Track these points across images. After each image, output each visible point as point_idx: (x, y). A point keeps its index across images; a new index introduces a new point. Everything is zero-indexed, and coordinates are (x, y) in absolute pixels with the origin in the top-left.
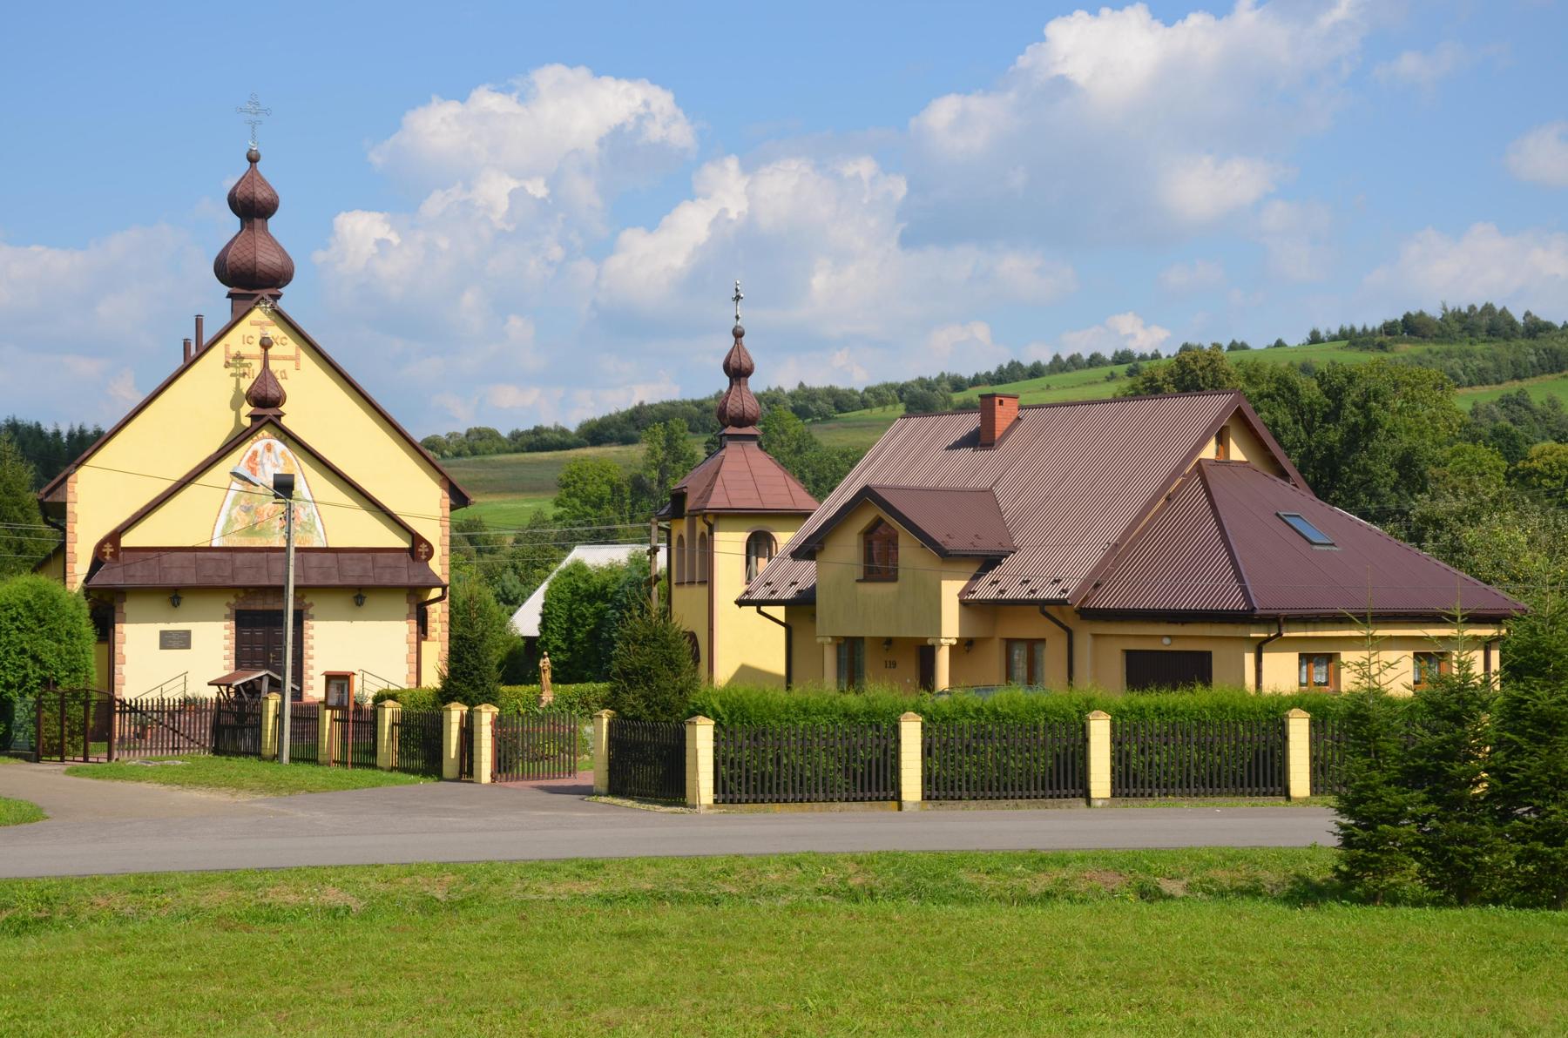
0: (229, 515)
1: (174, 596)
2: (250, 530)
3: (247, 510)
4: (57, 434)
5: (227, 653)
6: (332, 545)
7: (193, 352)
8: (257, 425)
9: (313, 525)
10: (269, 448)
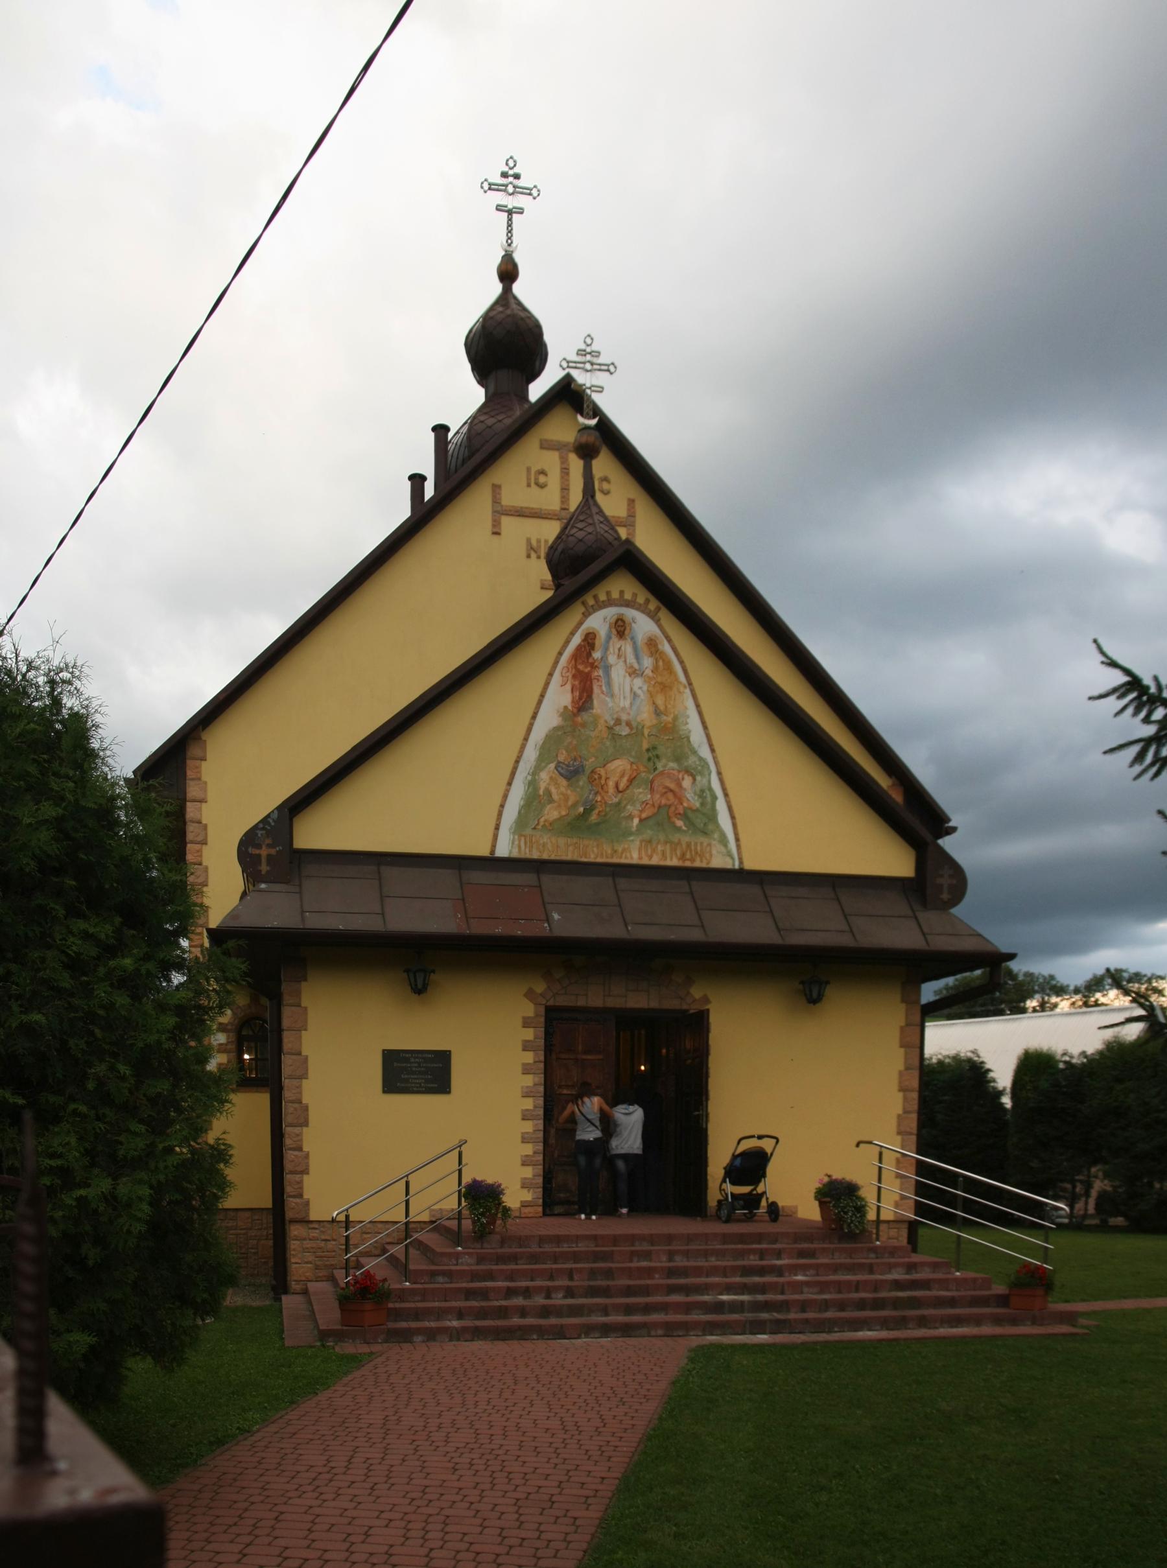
0: (532, 784)
1: (416, 961)
2: (579, 823)
3: (571, 773)
4: (994, 1081)
5: (529, 1104)
6: (749, 865)
7: (429, 491)
8: (570, 584)
9: (712, 817)
10: (620, 628)
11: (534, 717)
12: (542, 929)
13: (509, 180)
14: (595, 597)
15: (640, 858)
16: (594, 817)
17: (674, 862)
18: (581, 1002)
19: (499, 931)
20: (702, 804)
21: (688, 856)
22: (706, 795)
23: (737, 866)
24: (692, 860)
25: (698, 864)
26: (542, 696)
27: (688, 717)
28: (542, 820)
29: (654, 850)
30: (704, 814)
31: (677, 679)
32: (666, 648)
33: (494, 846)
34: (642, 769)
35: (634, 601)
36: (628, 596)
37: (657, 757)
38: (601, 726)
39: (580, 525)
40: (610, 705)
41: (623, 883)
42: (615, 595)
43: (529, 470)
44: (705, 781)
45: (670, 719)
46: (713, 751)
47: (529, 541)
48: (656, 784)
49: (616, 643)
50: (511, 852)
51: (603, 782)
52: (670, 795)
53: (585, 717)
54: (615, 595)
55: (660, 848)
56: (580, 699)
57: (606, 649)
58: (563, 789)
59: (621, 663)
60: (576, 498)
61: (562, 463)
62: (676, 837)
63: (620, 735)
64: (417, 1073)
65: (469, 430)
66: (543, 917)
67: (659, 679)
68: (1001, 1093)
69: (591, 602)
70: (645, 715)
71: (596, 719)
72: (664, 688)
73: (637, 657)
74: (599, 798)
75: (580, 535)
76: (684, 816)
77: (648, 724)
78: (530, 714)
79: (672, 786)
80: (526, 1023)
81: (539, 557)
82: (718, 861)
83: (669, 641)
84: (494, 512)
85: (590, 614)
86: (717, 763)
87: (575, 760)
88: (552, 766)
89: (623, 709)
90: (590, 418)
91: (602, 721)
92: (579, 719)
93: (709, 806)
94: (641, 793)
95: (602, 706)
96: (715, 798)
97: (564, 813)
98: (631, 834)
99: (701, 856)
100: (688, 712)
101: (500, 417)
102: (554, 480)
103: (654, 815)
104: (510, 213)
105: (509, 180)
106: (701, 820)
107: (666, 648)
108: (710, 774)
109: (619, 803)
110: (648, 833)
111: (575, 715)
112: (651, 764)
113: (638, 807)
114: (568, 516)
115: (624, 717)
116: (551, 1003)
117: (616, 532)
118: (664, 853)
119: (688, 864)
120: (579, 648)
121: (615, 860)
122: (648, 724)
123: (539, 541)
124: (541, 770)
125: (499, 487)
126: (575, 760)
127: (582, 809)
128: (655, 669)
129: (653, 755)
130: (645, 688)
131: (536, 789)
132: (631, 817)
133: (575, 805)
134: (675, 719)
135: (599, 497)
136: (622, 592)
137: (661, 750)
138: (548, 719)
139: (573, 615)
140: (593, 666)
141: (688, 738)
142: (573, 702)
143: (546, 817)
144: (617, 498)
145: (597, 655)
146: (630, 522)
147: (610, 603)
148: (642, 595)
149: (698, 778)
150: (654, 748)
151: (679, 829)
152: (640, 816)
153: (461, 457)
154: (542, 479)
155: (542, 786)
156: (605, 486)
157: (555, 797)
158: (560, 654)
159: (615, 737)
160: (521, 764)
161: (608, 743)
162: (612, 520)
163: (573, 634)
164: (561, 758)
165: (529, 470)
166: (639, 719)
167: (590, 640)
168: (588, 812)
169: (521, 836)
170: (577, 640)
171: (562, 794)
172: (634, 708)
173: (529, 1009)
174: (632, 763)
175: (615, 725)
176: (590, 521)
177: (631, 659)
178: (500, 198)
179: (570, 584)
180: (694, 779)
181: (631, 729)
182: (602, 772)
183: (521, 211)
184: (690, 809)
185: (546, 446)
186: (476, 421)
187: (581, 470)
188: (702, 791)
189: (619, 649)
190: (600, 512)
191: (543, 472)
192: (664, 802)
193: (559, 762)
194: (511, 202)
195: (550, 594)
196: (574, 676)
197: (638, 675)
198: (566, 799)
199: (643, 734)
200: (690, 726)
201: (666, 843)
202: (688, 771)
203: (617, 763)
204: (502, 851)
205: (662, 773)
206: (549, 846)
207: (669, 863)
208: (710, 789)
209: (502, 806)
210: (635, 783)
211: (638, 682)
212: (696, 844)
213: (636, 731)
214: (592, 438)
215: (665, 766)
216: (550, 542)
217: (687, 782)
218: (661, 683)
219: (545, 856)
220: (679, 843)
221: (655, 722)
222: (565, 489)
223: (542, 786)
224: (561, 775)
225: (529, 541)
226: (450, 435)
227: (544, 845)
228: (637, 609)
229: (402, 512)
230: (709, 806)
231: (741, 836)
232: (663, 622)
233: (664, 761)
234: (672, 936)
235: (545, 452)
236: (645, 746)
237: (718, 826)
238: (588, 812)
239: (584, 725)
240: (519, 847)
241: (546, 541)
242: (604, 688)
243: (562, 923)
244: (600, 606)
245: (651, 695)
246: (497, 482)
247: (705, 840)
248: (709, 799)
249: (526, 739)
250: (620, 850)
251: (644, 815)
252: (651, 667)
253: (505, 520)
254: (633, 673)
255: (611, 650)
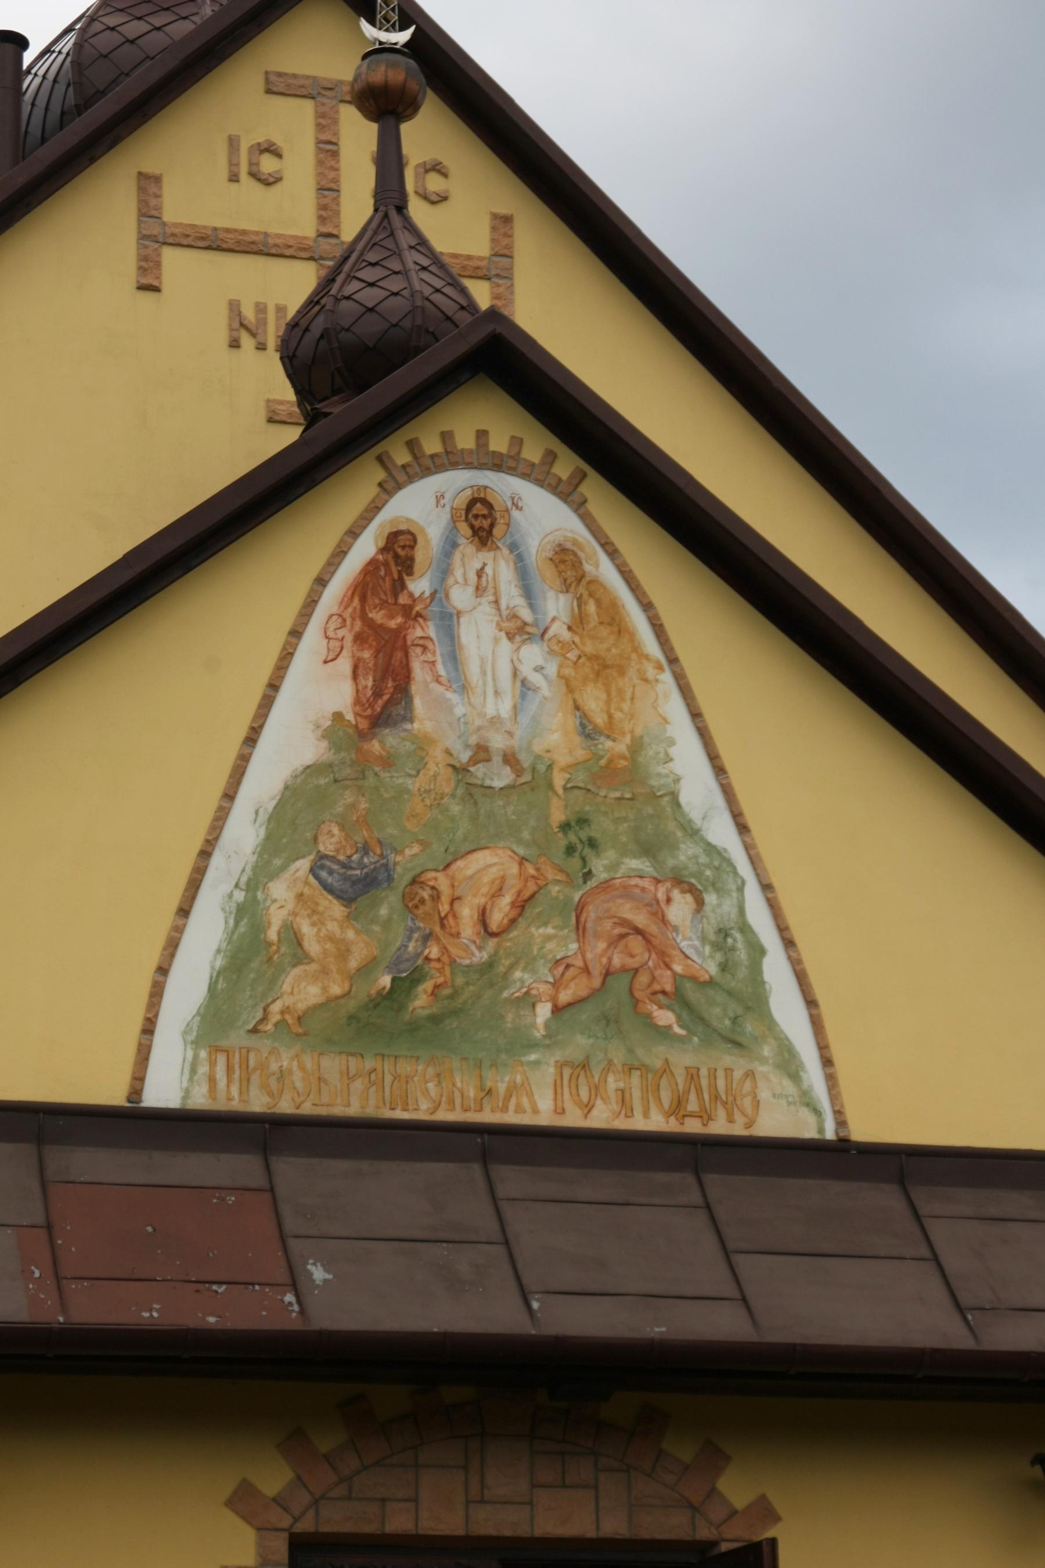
0: (248, 912)
2: (380, 1018)
3: (356, 884)
6: (865, 1130)
8: (345, 412)
9: (754, 1000)
10: (481, 521)
11: (252, 739)
12: (276, 1311)
14: (412, 445)
15: (560, 1111)
16: (421, 1001)
17: (656, 1122)
18: (399, 1522)
19: (151, 1314)
20: (724, 967)
21: (693, 1106)
22: (730, 938)
23: (830, 1134)
24: (705, 1116)
25: (719, 1127)
26: (274, 687)
27: (672, 742)
28: (276, 1007)
29: (596, 1090)
30: (730, 993)
31: (637, 649)
32: (607, 571)
33: (139, 1079)
34: (550, 874)
35: (516, 457)
36: (498, 444)
37: (592, 843)
38: (436, 763)
39: (369, 274)
40: (459, 710)
41: (513, 1179)
42: (465, 441)
43: (233, 143)
44: (728, 907)
45: (621, 747)
46: (743, 829)
47: (234, 307)
48: (591, 913)
49: (470, 559)
50: (185, 1098)
51: (444, 908)
52: (636, 944)
53: (390, 739)
54: (465, 441)
55: (613, 1083)
56: (377, 694)
57: (445, 572)
58: (332, 927)
59: (485, 606)
60: (356, 210)
61: (320, 127)
62: (655, 1055)
63: (485, 789)
65: (78, 46)
66: (281, 1275)
67: (589, 648)
68: (670, 1027)
69: (401, 457)
70: (554, 738)
71: (422, 744)
72: (604, 669)
73: (528, 593)
74: (434, 951)
75: (370, 296)
76: (676, 998)
77: (563, 759)
78: (242, 732)
79: (640, 919)
81: (261, 347)
82: (778, 1120)
83: (613, 553)
84: (142, 237)
85: (399, 487)
86: (755, 861)
87: (366, 849)
88: (303, 865)
89: (495, 721)
90: (392, 28)
91: (438, 753)
92: (375, 746)
93: (742, 973)
94: (550, 938)
95: (438, 713)
96: (758, 951)
97: (336, 990)
98: (532, 1045)
99: (731, 1109)
100: (671, 731)
101: (157, 21)
102: (299, 167)
103: (594, 993)
106: (725, 1009)
107: (607, 571)
108: (741, 889)
109: (490, 965)
110: (580, 1044)
111: (363, 736)
112: (575, 862)
113: (544, 972)
114: (338, 253)
115: (498, 742)
116: (306, 1525)
117: (463, 291)
118: (623, 1096)
119: (693, 1127)
120: (371, 568)
121: (488, 1116)
122: (563, 759)
123: (261, 309)
124: (273, 876)
125: (157, 180)
126: (366, 849)
127: (386, 981)
128: (578, 623)
129: (579, 839)
130: (552, 669)
131: (258, 927)
132: (528, 1000)
133: (367, 969)
134: (637, 746)
135: (417, 210)
136: (482, 435)
137: (601, 826)
138: (291, 745)
139: (353, 489)
140: (411, 614)
141: (674, 796)
142: (357, 701)
143: (288, 1001)
144: (463, 209)
145: (419, 586)
146: (499, 267)
147: (451, 459)
148: (538, 443)
149: (711, 898)
150: (583, 821)
151: (664, 1033)
152: (554, 1000)
153: (56, 108)
154: (268, 164)
155: (276, 918)
156: (434, 183)
157: (313, 947)
158: (321, 582)
159: (473, 792)
160: (217, 860)
161: (456, 809)
162: (447, 260)
163: (354, 533)
164: (327, 846)
165: (233, 143)
166: (538, 747)
167: (400, 549)
168: (405, 984)
169: (215, 1050)
170: (365, 548)
171: (331, 938)
172: (524, 719)
174: (522, 860)
175: (474, 761)
176: (396, 266)
177: (511, 596)
179: (345, 412)
180: (700, 903)
181: (518, 771)
182: (442, 882)
184: (694, 979)
185: (280, 86)
186: (97, 27)
187: (373, 146)
188: (724, 933)
189: (480, 573)
190: (422, 244)
191: (271, 149)
192: (617, 961)
193: (322, 857)
195: (291, 435)
196: (359, 639)
197: (530, 638)
198: (344, 952)
199: (550, 786)
200: (677, 767)
201: (630, 1069)
202: (678, 881)
203: (482, 859)
204: (164, 1091)
205: (606, 886)
206: (297, 1077)
207: (639, 1123)
208: (745, 928)
209: (163, 971)
210: (531, 912)
211: (532, 654)
212: (713, 1074)
213: (532, 778)
214: (397, 73)
215: (614, 867)
216: (291, 313)
217: (679, 910)
218: (593, 658)
219: (285, 1106)
220: (666, 1069)
221: (581, 754)
222: (328, 191)
223: (276, 918)
224: (329, 889)
225: (234, 307)
226: (28, 57)
227: (283, 1075)
228: (524, 476)
230: (742, 973)
231: (837, 1053)
232: (592, 507)
233: (610, 855)
234: (657, 1329)
235: (269, 96)
236: (558, 816)
237: (771, 1025)
238: (405, 984)
239: (388, 762)
240: (212, 1080)
241: (281, 310)
242: (441, 669)
243: (338, 1292)
244: (425, 466)
245: (569, 686)
246: (150, 167)
247: (739, 1064)
248: (742, 955)
249: (229, 796)
250: (502, 1088)
251: (565, 997)
252: (565, 617)
253: (170, 257)
254: (518, 631)
255: (458, 573)
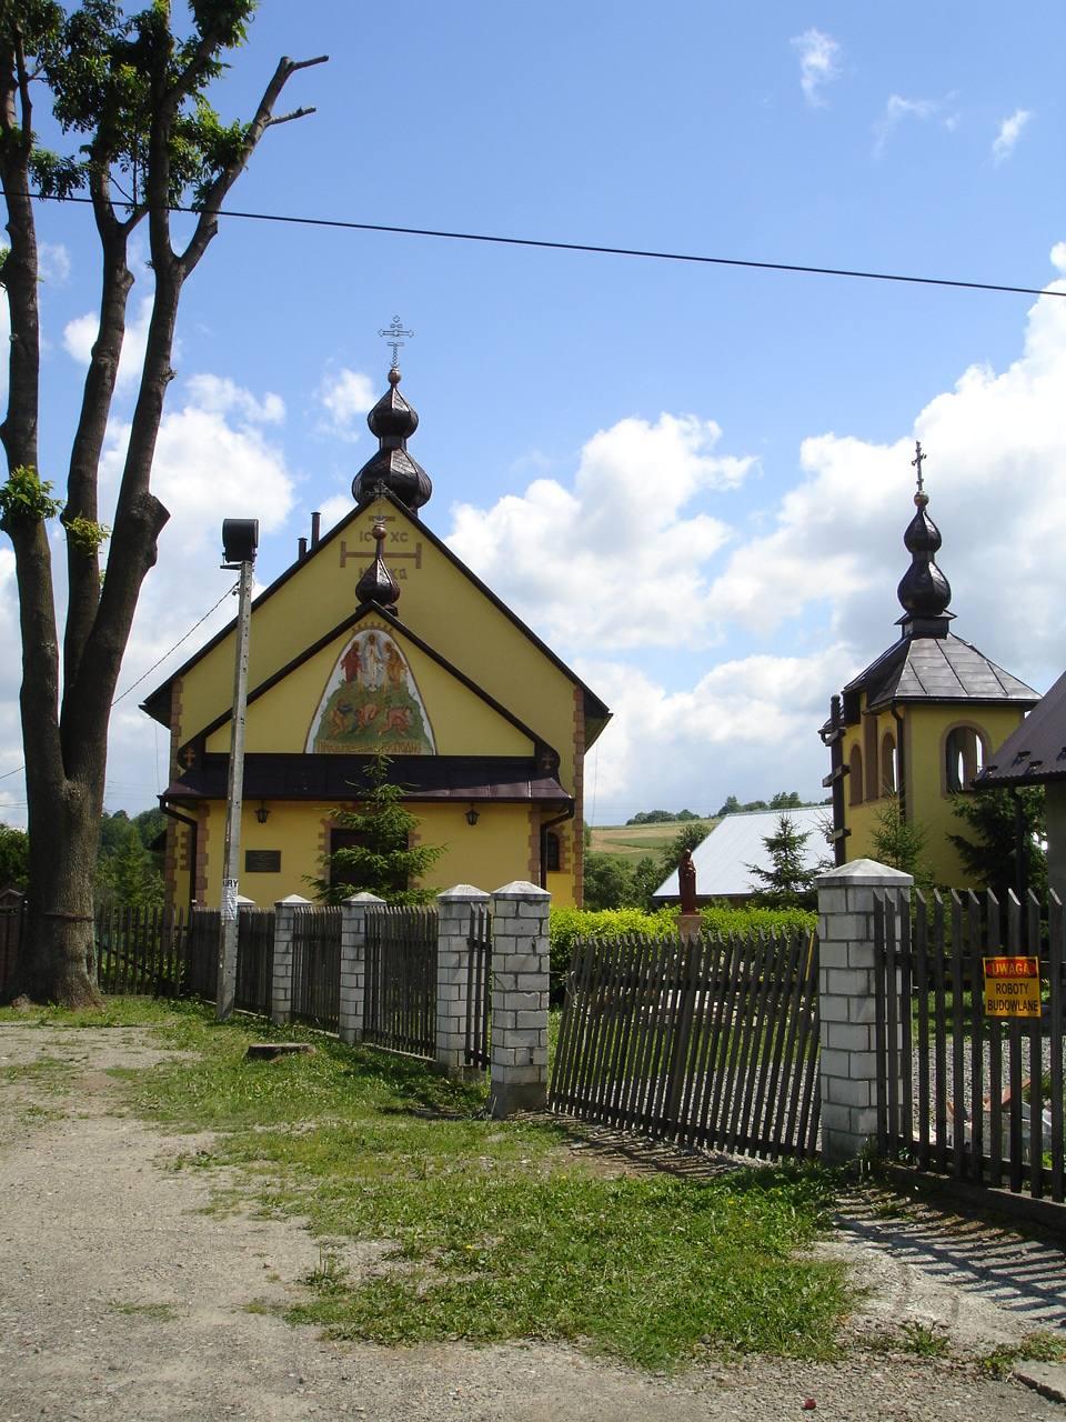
10: (372, 640)
13: (396, 330)
22: (418, 719)
42: (369, 624)
43: (361, 533)
49: (369, 647)
64: (263, 862)
80: (321, 836)
104: (396, 345)
105: (396, 330)
106: (415, 731)
138: (334, 685)
145: (359, 654)
147: (366, 628)
148: (383, 623)
151: (402, 736)
170: (349, 648)
173: (322, 829)
177: (377, 654)
178: (388, 338)
183: (403, 344)
194: (396, 340)
229: (295, 558)
236: (385, 696)
237: (424, 735)
244: (361, 629)
254: (378, 661)
